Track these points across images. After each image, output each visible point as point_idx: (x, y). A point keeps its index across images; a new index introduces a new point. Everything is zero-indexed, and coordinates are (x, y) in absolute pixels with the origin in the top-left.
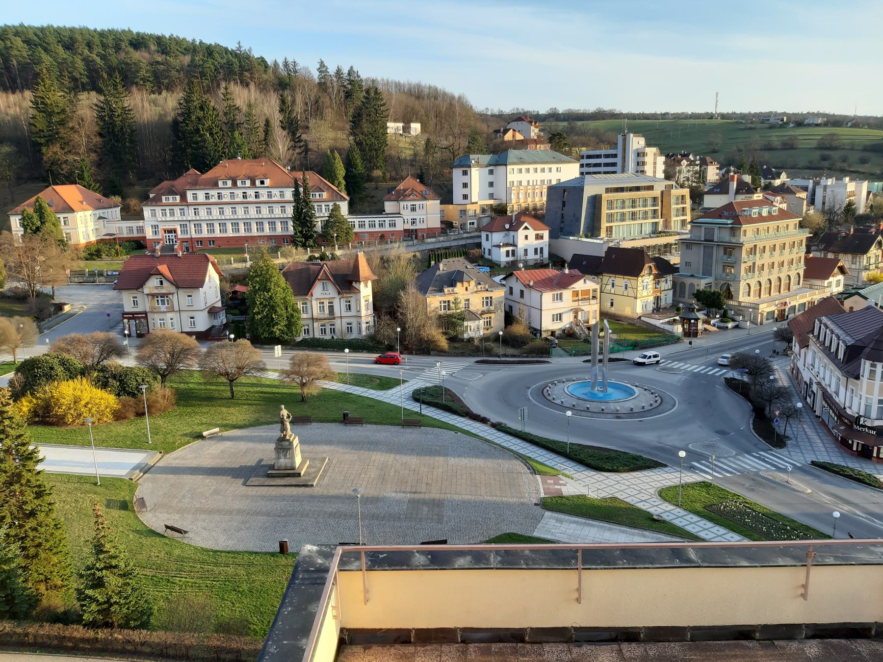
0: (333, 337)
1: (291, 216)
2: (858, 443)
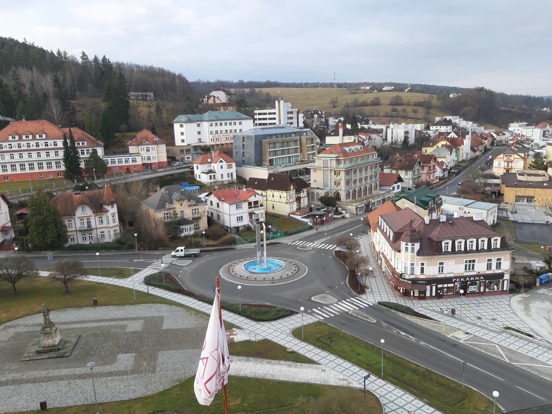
0: (91, 242)
1: (62, 158)
2: (403, 289)
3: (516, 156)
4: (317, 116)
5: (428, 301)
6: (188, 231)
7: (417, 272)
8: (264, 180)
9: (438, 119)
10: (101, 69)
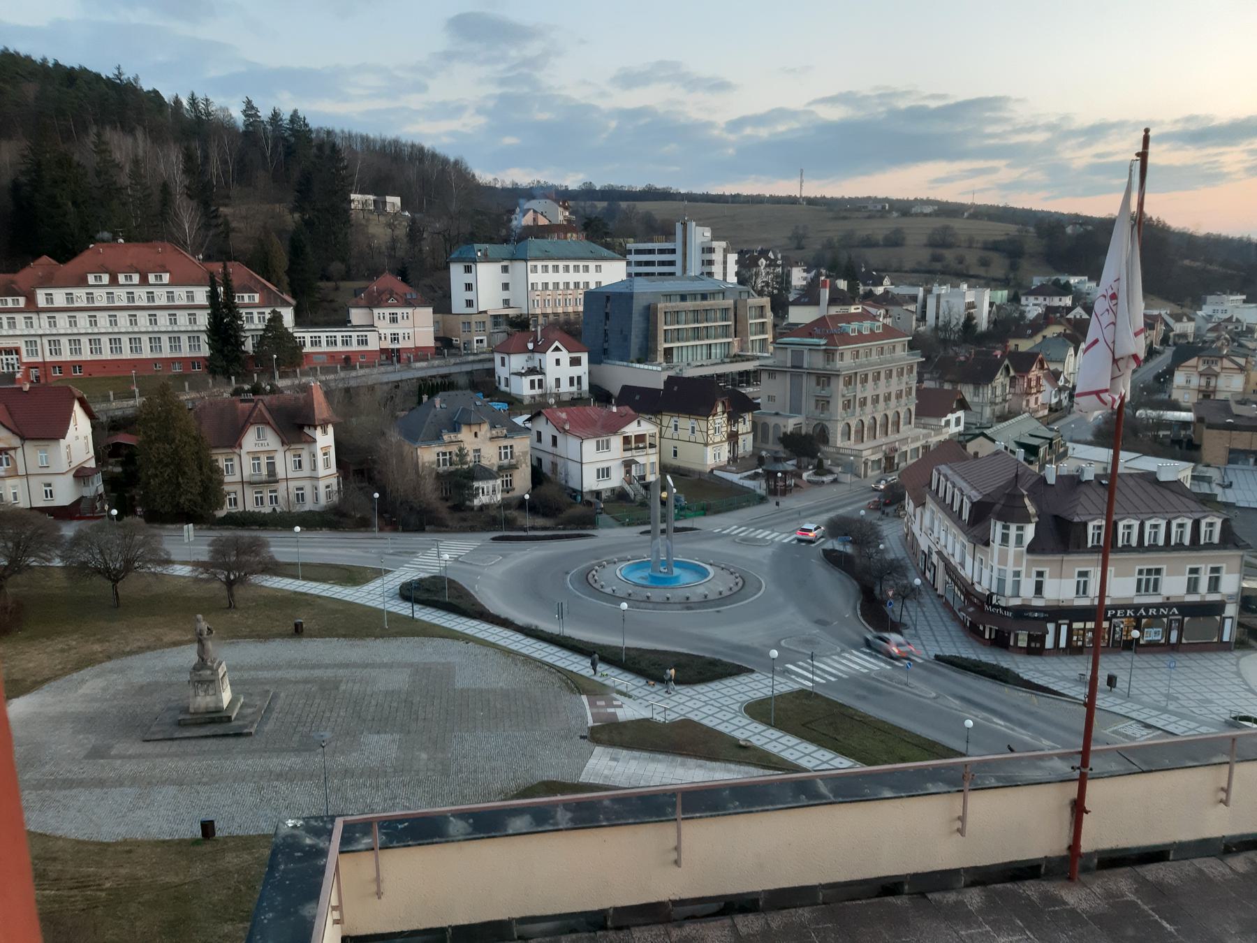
0: (274, 509)
1: (204, 328)
2: (991, 629)
3: (1226, 363)
4: (764, 262)
5: (1048, 659)
6: (488, 493)
7: (1027, 589)
8: (655, 391)
9: (1037, 281)
10: (285, 139)
